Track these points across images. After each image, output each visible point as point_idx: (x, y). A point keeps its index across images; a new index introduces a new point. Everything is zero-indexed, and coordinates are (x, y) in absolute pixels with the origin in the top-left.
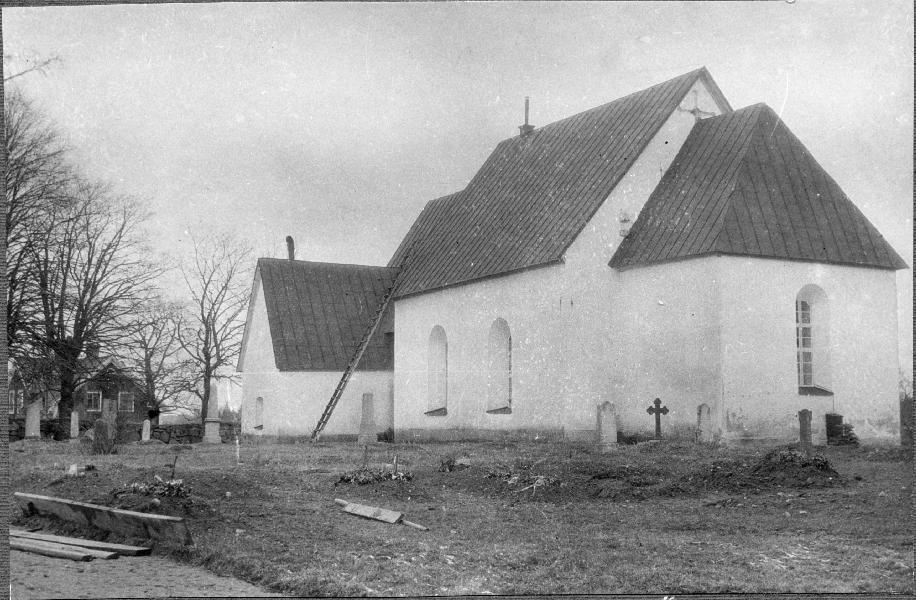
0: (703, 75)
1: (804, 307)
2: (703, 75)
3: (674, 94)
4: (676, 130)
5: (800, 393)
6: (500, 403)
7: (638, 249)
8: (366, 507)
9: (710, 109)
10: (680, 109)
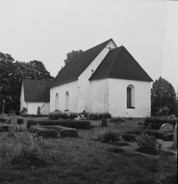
0: (111, 40)
1: (129, 90)
2: (111, 40)
7: (95, 77)
9: (113, 47)
10: (106, 47)
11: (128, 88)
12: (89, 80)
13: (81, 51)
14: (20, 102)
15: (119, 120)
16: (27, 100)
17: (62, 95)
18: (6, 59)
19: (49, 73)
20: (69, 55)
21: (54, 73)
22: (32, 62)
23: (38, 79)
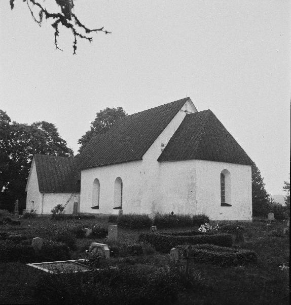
0: (188, 99)
1: (223, 176)
3: (176, 106)
4: (179, 118)
5: (221, 206)
6: (118, 205)
7: (167, 156)
8: (175, 204)
16: (45, 189)
20: (100, 116)
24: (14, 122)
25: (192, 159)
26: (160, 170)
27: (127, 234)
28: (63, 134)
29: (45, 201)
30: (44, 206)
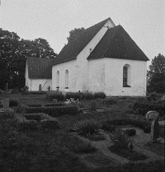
0: (109, 19)
1: (125, 69)
2: (109, 19)
5: (123, 87)
7: (93, 56)
9: (111, 26)
11: (124, 67)
12: (87, 59)
13: (83, 28)
14: (25, 78)
15: (113, 101)
16: (31, 77)
17: (63, 73)
18: (13, 37)
19: (53, 50)
20: (72, 33)
21: (57, 50)
22: (37, 40)
23: (40, 57)
24: (22, 39)
25: (102, 57)
26: (89, 64)
27: (39, 103)
28: (52, 46)
29: (32, 84)
30: (32, 86)
